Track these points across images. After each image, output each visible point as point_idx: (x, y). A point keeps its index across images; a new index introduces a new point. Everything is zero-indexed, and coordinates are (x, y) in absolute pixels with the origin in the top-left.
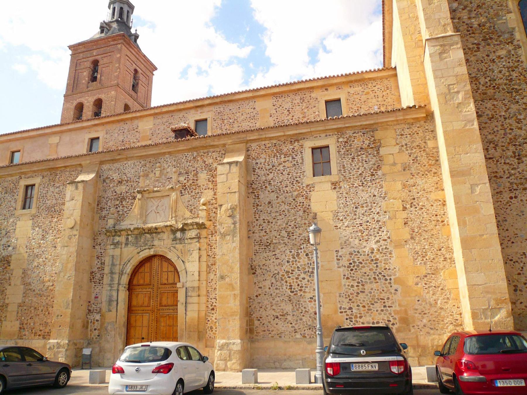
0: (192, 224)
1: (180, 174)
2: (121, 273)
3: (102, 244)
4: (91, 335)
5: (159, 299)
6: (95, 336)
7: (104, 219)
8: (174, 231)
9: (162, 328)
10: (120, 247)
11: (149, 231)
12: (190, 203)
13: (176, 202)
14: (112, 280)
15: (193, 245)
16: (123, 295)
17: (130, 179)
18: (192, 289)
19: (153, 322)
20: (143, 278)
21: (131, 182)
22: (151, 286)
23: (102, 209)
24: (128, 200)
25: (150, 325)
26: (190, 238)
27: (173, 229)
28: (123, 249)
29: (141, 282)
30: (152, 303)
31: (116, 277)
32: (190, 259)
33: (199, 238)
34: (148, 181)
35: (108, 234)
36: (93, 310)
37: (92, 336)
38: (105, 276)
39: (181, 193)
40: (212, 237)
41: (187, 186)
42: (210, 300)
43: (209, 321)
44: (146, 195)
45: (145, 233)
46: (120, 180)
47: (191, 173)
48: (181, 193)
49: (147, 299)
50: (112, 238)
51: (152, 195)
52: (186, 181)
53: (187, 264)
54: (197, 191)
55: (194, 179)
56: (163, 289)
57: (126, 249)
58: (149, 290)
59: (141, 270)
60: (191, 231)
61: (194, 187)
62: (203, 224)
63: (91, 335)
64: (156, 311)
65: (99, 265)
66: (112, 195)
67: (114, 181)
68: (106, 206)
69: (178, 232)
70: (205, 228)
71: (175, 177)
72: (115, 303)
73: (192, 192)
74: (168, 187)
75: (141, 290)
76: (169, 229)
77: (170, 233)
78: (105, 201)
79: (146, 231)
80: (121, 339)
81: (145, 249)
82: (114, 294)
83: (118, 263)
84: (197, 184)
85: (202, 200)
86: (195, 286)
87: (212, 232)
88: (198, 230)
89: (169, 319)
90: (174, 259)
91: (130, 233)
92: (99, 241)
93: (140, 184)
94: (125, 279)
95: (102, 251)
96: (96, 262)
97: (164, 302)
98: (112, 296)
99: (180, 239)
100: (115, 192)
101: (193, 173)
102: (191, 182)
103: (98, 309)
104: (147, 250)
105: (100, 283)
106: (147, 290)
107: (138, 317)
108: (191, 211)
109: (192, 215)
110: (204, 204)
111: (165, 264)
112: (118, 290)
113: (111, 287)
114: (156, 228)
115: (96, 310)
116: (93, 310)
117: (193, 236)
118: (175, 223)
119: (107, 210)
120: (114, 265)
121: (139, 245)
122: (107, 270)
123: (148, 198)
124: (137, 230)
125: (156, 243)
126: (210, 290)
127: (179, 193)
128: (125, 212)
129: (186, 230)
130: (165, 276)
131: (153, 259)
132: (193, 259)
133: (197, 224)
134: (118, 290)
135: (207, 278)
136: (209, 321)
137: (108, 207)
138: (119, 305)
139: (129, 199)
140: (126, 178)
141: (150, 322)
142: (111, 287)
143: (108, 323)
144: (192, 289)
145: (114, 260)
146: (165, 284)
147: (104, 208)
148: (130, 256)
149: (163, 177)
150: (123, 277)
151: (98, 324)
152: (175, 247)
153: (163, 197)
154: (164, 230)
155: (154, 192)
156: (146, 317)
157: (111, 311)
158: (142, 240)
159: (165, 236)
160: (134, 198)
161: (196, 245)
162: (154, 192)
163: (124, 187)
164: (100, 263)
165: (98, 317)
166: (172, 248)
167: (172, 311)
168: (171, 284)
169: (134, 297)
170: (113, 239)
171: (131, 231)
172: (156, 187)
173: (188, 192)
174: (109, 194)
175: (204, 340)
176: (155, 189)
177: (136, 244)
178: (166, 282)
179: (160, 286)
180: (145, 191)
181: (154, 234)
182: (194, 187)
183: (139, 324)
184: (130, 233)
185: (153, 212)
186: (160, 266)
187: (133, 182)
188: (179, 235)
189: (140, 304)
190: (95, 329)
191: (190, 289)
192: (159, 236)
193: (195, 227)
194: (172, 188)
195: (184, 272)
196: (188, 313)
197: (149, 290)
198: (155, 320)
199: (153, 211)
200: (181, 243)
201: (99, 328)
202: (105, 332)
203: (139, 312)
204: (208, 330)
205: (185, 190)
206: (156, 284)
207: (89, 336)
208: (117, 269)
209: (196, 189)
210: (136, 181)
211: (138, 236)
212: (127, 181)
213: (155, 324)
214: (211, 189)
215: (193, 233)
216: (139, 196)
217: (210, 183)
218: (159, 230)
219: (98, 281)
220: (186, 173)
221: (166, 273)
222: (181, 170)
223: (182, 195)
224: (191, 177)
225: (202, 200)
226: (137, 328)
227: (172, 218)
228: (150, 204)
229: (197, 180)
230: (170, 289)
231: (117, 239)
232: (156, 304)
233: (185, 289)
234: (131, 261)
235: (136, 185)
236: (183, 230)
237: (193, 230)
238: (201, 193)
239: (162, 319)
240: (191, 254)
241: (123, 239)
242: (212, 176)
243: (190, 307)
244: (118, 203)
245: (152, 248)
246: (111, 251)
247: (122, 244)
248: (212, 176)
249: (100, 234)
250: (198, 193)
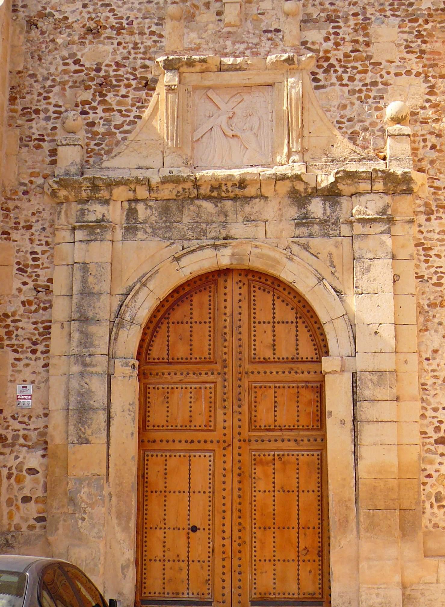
0: (371, 177)
1: (307, 21)
2: (118, 321)
3: (36, 227)
4: (11, 516)
5: (246, 408)
6: (27, 520)
7: (38, 147)
8: (300, 194)
9: (259, 496)
10: (109, 236)
11: (213, 189)
12: (348, 113)
13: (303, 105)
14: (87, 340)
15: (371, 243)
16: (126, 392)
17: (131, 23)
18: (375, 378)
19: (228, 480)
20: (191, 336)
21: (132, 33)
22: (218, 367)
23: (28, 113)
24: (123, 91)
25: (218, 486)
26: (360, 221)
27: (301, 187)
28: (118, 245)
29: (181, 351)
30: (220, 416)
31: (101, 332)
32: (364, 283)
33: (391, 221)
34: (193, 35)
35: (63, 193)
36: (16, 437)
37: (16, 520)
38: (55, 329)
39: (316, 80)
40: (429, 220)
41: (333, 61)
42: (430, 413)
43: (429, 476)
44: (193, 78)
45: (197, 198)
46: (92, 25)
47: (346, 21)
48: (316, 80)
49: (203, 406)
50: (75, 207)
51: (212, 79)
52: (330, 45)
53: (353, 302)
54: (369, 78)
55: (357, 41)
56: (260, 377)
57: (130, 244)
58: (211, 378)
59: (178, 314)
60: (363, 198)
61: (357, 64)
62: (406, 179)
63: (11, 516)
64: (236, 444)
65: (28, 294)
66: (65, 72)
67: (69, 27)
68: (42, 106)
69: (314, 204)
70: (409, 191)
71: (291, 30)
72: (102, 416)
73: (351, 79)
74: (271, 58)
75: (179, 377)
76: (284, 187)
77: (287, 201)
78: (37, 87)
79: (204, 190)
80: (126, 529)
81: (201, 248)
82: (98, 386)
83: (106, 287)
84: (369, 57)
85: (392, 108)
86: (383, 367)
87: (427, 204)
88: (387, 199)
89: (284, 470)
90: (304, 284)
91: (142, 192)
92: (24, 216)
93: (165, 42)
94: (130, 339)
95: (39, 249)
96: (17, 284)
97: (265, 416)
98: (90, 391)
99: (323, 223)
100: (77, 62)
101: (352, 22)
102: (347, 48)
103: (34, 435)
104: (209, 252)
105: (34, 352)
106: (204, 378)
107: (172, 462)
108: (353, 137)
109: (358, 150)
110: (397, 120)
111: (264, 300)
112: (109, 376)
113: (85, 365)
114: (242, 184)
115: (25, 437)
116: (16, 437)
117: (371, 214)
118: (304, 170)
119: (48, 119)
120: (90, 294)
121: (176, 235)
122: (61, 310)
123: (196, 88)
124: (170, 186)
125: (237, 229)
126: (430, 382)
127: (308, 78)
128: (117, 127)
129: (339, 194)
130: (264, 336)
131: (221, 281)
132: (375, 286)
133: (388, 177)
134: (109, 376)
135: (419, 345)
136: (429, 476)
137: (52, 109)
138: (114, 423)
139: (128, 86)
140: (113, 21)
141: (219, 478)
142: (85, 365)
143: (80, 481)
144: (375, 378)
145: (91, 279)
146: (266, 361)
147: (37, 112)
148: (146, 268)
149: (249, 26)
150: (123, 334)
151: (37, 481)
152: (306, 247)
153: (249, 88)
154: (268, 191)
155: (221, 68)
156: (202, 464)
157: (87, 442)
158: (186, 220)
159: (269, 210)
160: (149, 86)
161: (383, 243)
162: (221, 68)
163: (109, 48)
164: (31, 285)
165: (34, 460)
166: (296, 249)
167: (292, 444)
168: (287, 361)
169: (155, 398)
170: (83, 212)
171: (150, 189)
172: (226, 55)
173: (340, 79)
174: (53, 65)
175: (420, 534)
176: (229, 61)
177: (166, 228)
178: (268, 354)
179: (248, 367)
180: (190, 63)
181: (229, 203)
182: (357, 64)
183: (177, 482)
184: (142, 192)
185: (217, 131)
186: (245, 305)
187: (142, 33)
188: (317, 207)
189: (179, 422)
190: (26, 499)
191: (369, 376)
192: (247, 209)
193: (379, 186)
194: (290, 61)
195: (341, 324)
196: (363, 451)
197: (211, 378)
198: (236, 471)
199: (216, 130)
200: (327, 235)
201: (40, 493)
202: (71, 509)
203: (178, 446)
204: (427, 505)
205: (327, 71)
206: (232, 363)
207: (5, 521)
208: (104, 308)
209: (365, 72)
210: (153, 33)
211: (173, 206)
212: (119, 30)
213: (236, 485)
214: (418, 75)
215: (368, 206)
216: (169, 78)
217: (412, 56)
218: (250, 191)
219: (27, 344)
220: (329, 19)
221: (269, 328)
222: (310, 10)
223: (317, 88)
224: (346, 31)
225: (392, 108)
226: (172, 499)
227: (289, 155)
228: (154, 123)
229: (367, 44)
230: (281, 377)
231: (96, 211)
232: (236, 423)
233: (348, 376)
234: (151, 285)
235: (149, 43)
236: (332, 194)
237: (368, 197)
238: (386, 84)
239: (259, 470)
240: (368, 270)
241: (115, 213)
242: (419, 35)
243: (368, 434)
244: (87, 96)
245: (225, 246)
246: (74, 249)
247: (114, 229)
248: (419, 35)
249: (25, 193)
250: (374, 84)
